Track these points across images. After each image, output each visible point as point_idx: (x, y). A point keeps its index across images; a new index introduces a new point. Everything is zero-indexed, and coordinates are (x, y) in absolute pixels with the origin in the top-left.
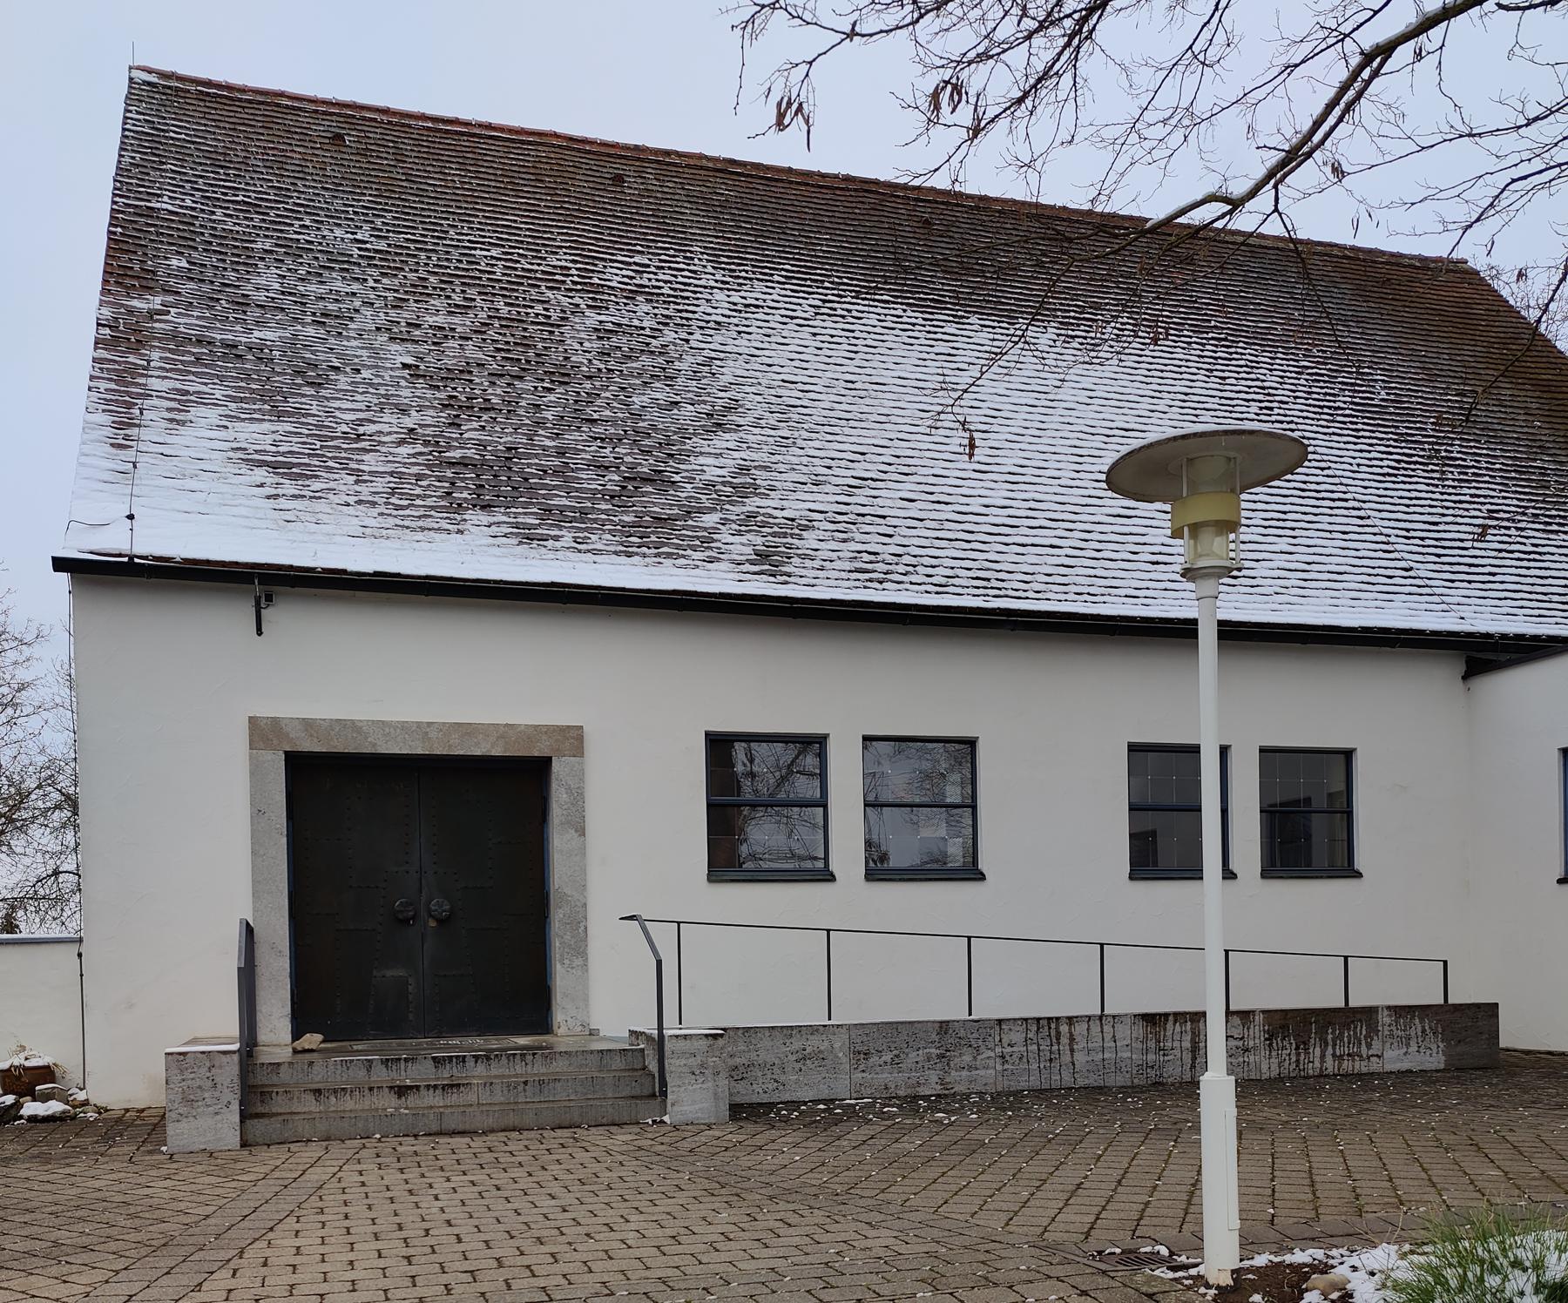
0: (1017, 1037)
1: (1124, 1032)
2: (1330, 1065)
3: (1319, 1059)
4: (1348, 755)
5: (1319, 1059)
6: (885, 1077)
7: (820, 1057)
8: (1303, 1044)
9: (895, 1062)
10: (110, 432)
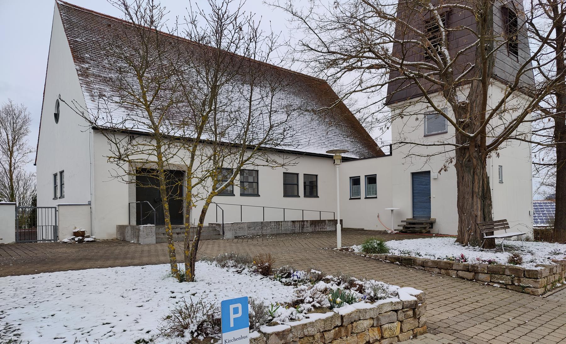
0: (273, 225)
1: (289, 224)
2: (319, 230)
3: (318, 229)
4: (317, 176)
5: (318, 229)
6: (253, 231)
7: (242, 228)
8: (315, 226)
9: (255, 229)
10: (90, 97)
